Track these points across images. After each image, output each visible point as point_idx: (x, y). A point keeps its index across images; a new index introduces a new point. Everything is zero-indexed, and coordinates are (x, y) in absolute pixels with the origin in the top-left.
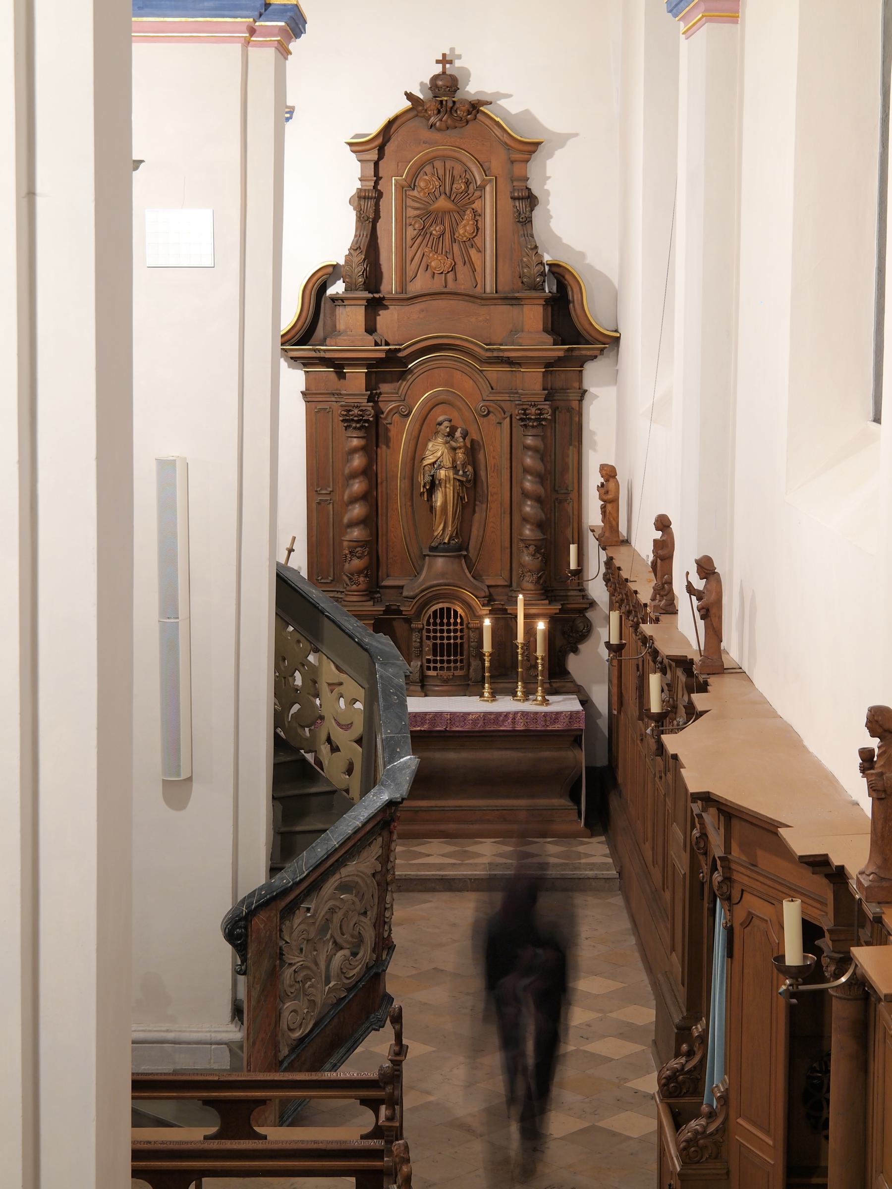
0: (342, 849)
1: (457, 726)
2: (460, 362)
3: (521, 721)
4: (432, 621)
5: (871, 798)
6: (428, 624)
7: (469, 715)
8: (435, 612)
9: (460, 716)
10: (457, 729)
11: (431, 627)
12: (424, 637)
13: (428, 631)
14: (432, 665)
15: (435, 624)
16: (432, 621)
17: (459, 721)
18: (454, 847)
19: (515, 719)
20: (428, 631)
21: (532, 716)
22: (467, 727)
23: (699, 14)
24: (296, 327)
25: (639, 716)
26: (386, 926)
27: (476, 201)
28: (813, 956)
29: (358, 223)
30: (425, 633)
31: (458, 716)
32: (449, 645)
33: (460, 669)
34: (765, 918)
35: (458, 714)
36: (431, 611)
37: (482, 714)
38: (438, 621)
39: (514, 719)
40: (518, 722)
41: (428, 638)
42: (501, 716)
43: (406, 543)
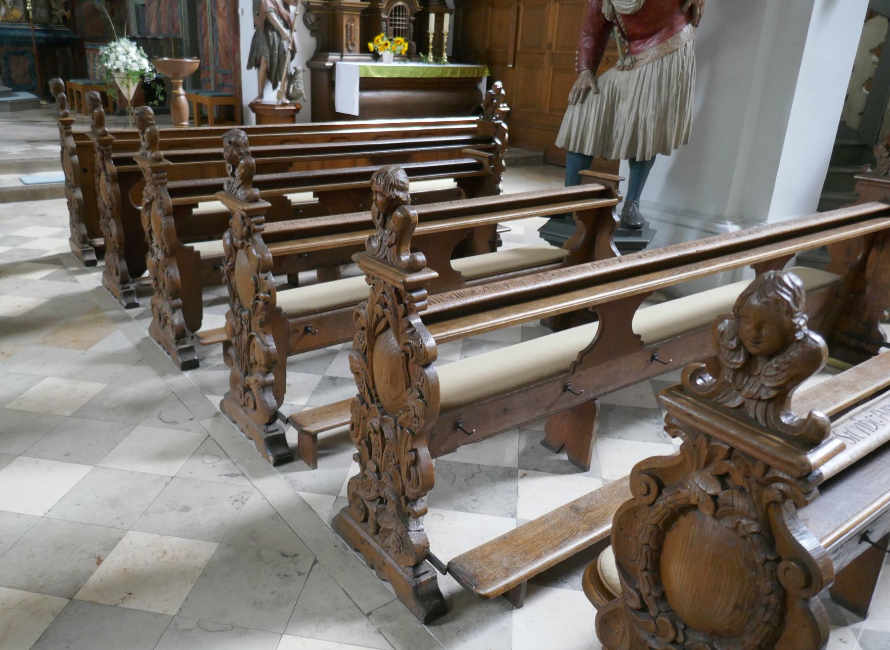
0: (120, 244)
4: (393, 14)
6: (391, 15)
8: (395, 8)
11: (393, 18)
12: (389, 25)
13: (391, 20)
14: (393, 23)
15: (395, 16)
16: (393, 14)
18: (188, 39)
20: (391, 20)
25: (125, 233)
26: (159, 270)
27: (164, 487)
28: (130, 199)
29: (412, 59)
30: (389, 22)
32: (399, 29)
33: (184, 331)
36: (393, 8)
38: (397, 14)
41: (391, 25)
43: (580, 144)
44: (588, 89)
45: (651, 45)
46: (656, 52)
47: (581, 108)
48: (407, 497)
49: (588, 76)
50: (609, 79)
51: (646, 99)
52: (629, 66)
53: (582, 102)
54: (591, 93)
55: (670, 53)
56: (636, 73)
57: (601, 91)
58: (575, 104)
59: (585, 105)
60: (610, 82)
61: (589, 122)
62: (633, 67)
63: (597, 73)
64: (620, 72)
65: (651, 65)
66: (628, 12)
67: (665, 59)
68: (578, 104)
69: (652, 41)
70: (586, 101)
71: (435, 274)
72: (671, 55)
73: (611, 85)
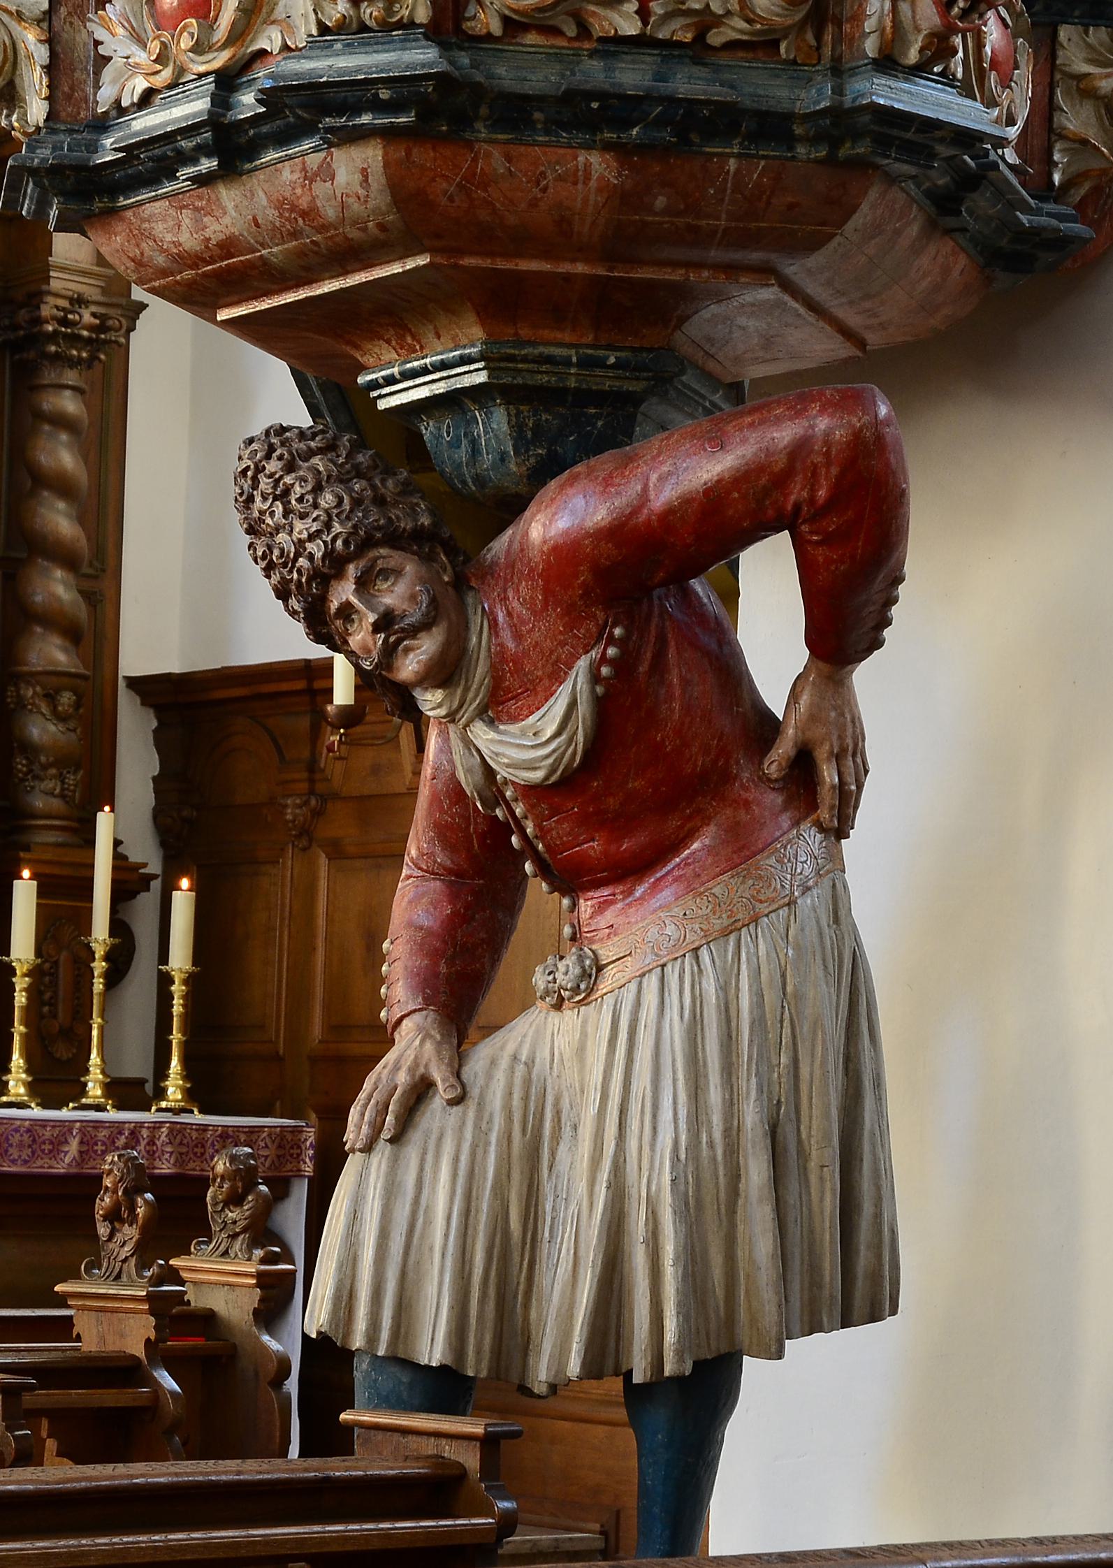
1: (14, 1162)
2: (467, 1213)
3: (169, 1149)
5: (788, 1343)
7: (44, 1127)
9: (22, 1130)
10: (14, 1169)
17: (21, 1145)
19: (154, 1144)
21: (194, 1135)
22: (39, 1163)
23: (420, 252)
24: (859, 1207)
31: (17, 1130)
34: (9, 7)
35: (18, 1123)
37: (78, 1125)
39: (152, 1142)
40: (163, 1152)
42: (121, 1133)
44: (421, 1090)
45: (655, 902)
46: (670, 930)
47: (395, 1162)
48: (168, 973)
49: (427, 1036)
50: (510, 1048)
51: (648, 1117)
52: (576, 990)
53: (395, 1140)
54: (437, 1102)
55: (726, 933)
56: (599, 1017)
57: (474, 1092)
58: (368, 1149)
59: (411, 1153)
60: (515, 1058)
61: (428, 1222)
62: (590, 991)
63: (472, 1033)
64: (554, 1017)
65: (652, 982)
66: (537, 776)
67: (705, 955)
68: (383, 1150)
69: (655, 888)
70: (415, 1138)
71: (56, 1289)
72: (732, 938)
73: (520, 1070)
